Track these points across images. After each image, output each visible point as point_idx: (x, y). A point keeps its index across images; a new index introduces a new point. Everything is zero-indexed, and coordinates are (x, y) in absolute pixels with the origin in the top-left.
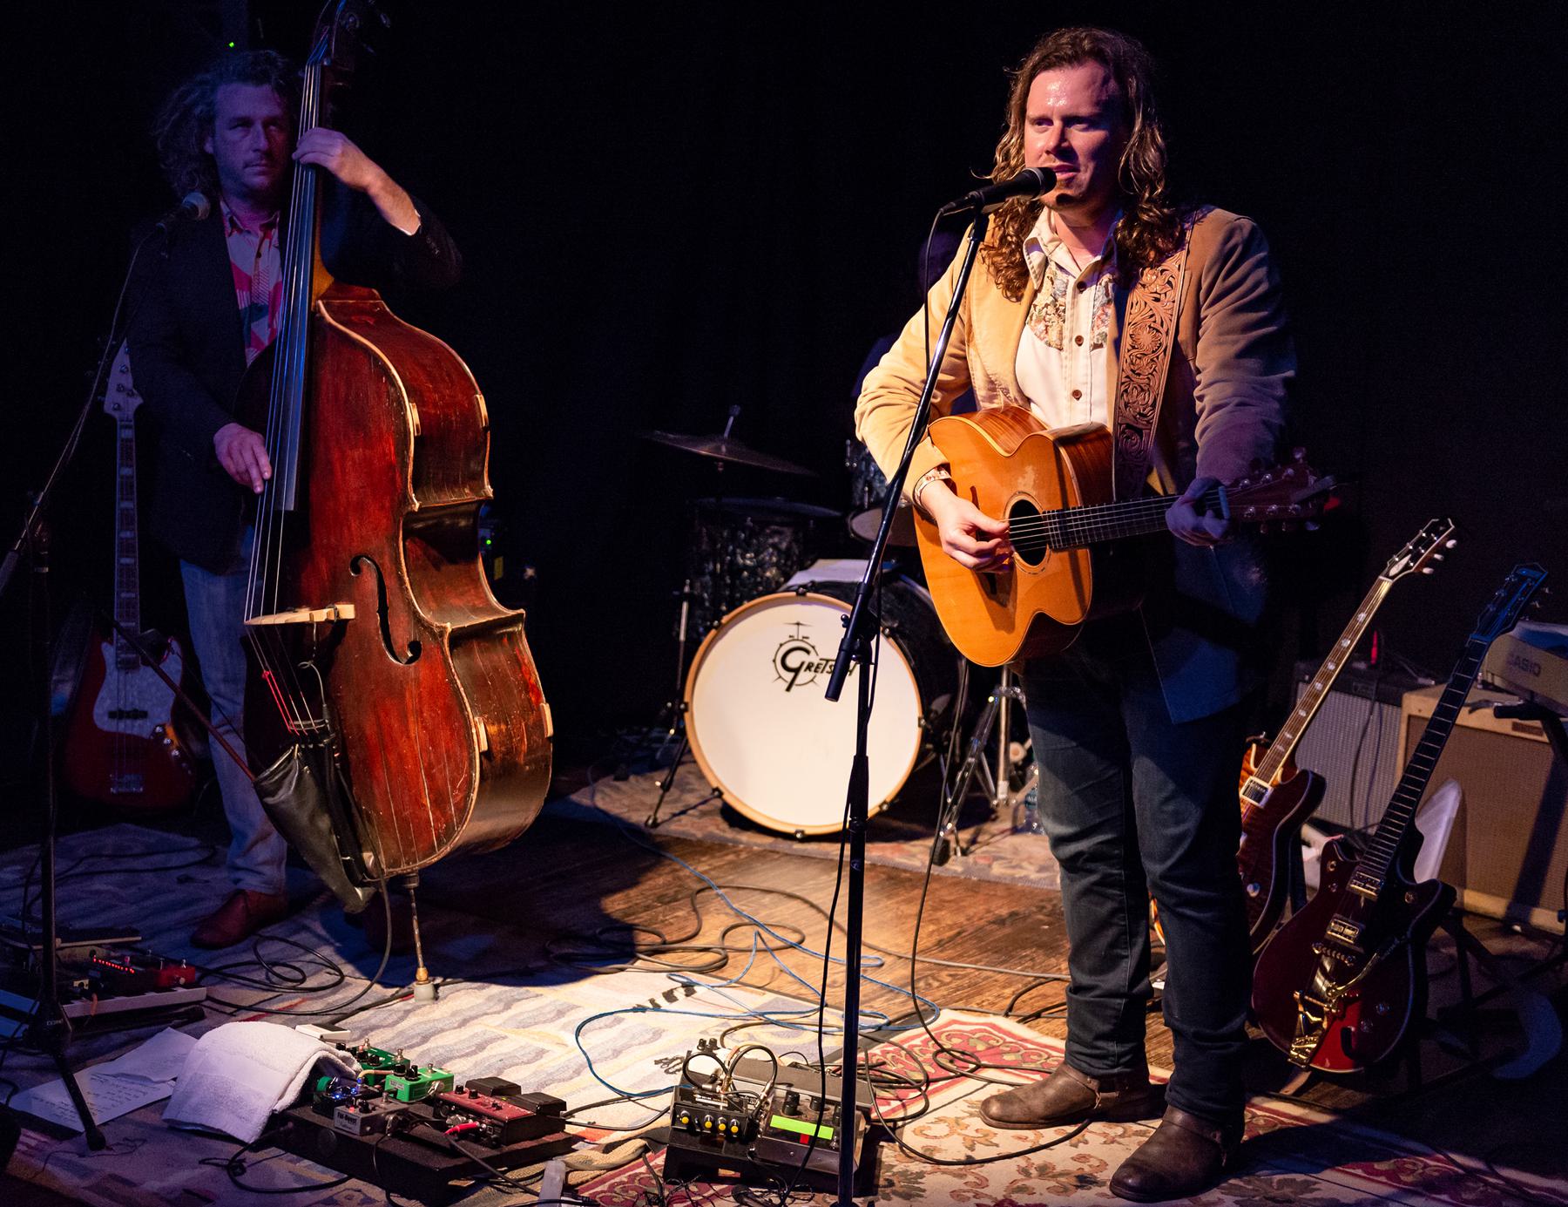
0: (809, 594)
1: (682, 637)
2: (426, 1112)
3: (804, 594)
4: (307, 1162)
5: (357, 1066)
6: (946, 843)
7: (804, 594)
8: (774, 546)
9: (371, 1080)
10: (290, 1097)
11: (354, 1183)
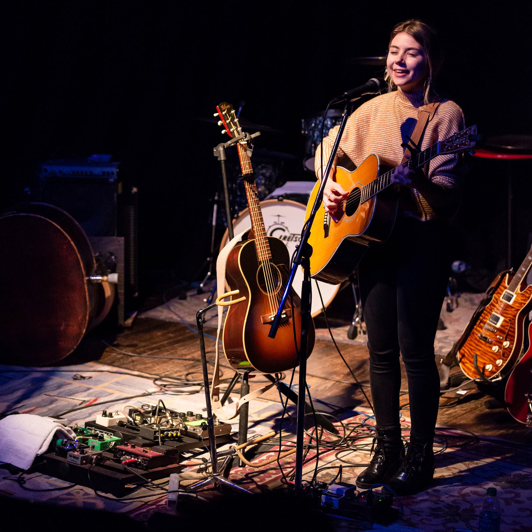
0: (285, 201)
1: (214, 223)
2: (110, 455)
3: (282, 200)
4: (54, 478)
5: (73, 435)
6: (356, 328)
7: (282, 200)
8: (263, 175)
9: (81, 441)
10: (45, 448)
11: (78, 487)
